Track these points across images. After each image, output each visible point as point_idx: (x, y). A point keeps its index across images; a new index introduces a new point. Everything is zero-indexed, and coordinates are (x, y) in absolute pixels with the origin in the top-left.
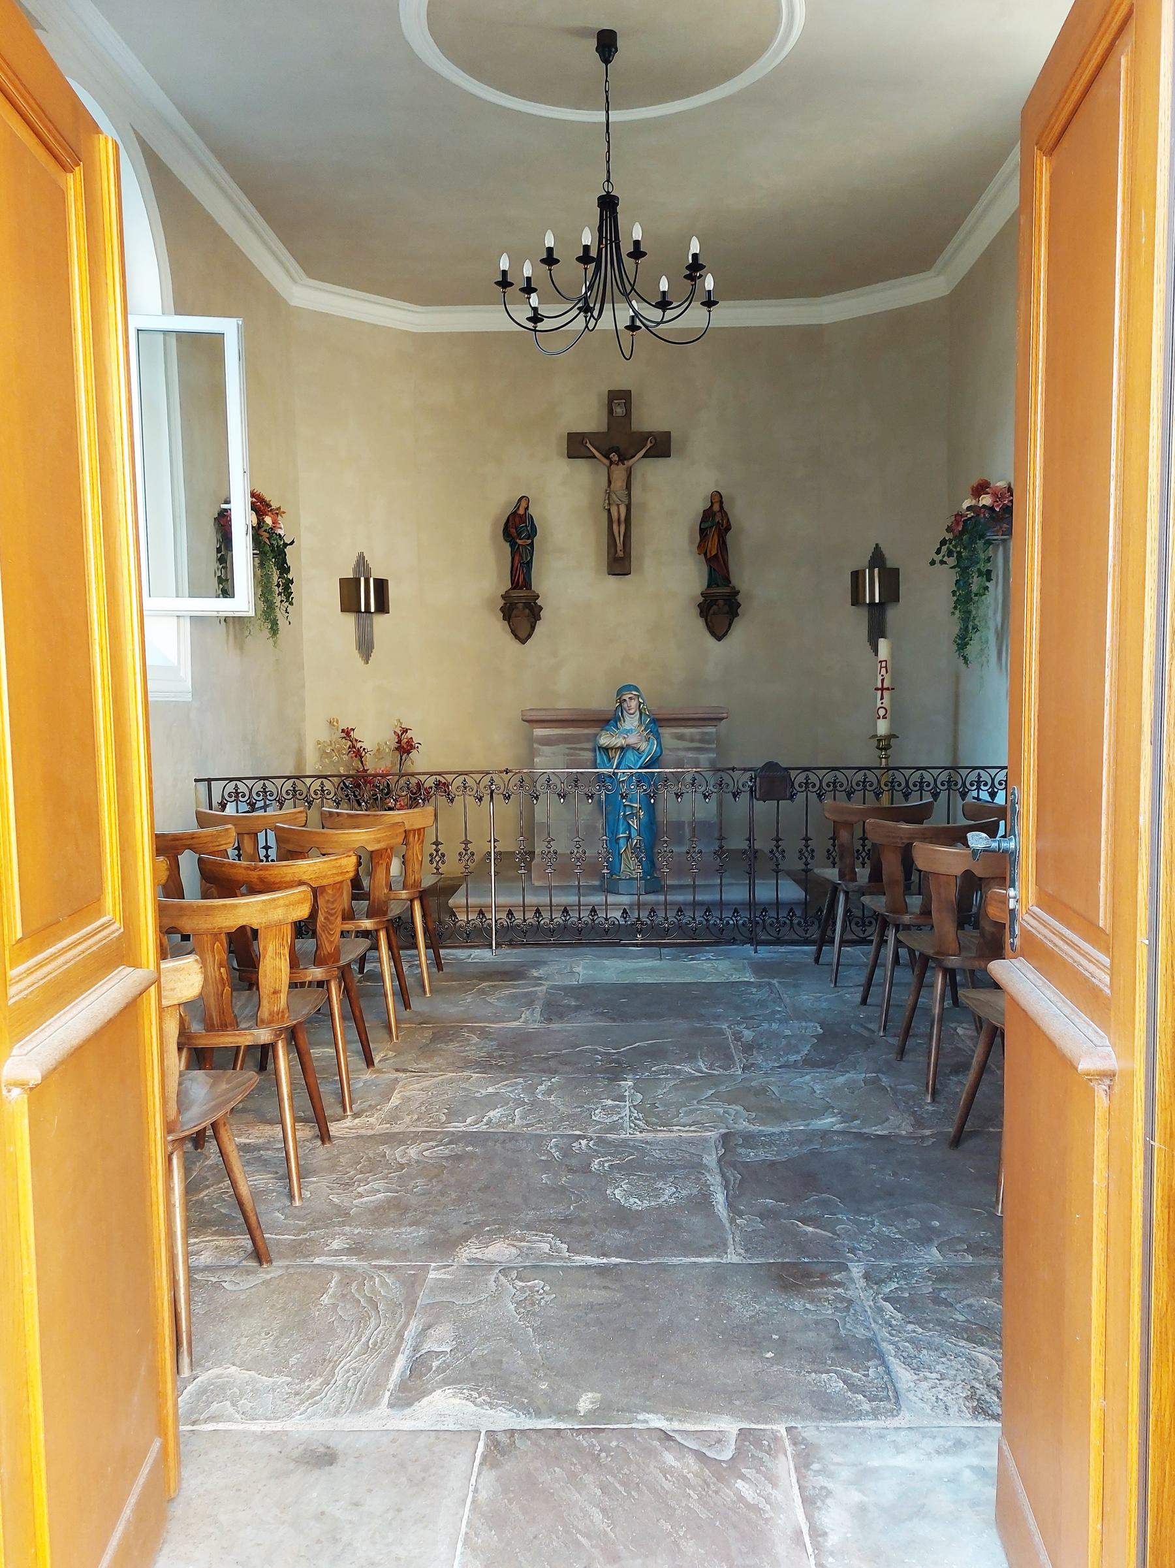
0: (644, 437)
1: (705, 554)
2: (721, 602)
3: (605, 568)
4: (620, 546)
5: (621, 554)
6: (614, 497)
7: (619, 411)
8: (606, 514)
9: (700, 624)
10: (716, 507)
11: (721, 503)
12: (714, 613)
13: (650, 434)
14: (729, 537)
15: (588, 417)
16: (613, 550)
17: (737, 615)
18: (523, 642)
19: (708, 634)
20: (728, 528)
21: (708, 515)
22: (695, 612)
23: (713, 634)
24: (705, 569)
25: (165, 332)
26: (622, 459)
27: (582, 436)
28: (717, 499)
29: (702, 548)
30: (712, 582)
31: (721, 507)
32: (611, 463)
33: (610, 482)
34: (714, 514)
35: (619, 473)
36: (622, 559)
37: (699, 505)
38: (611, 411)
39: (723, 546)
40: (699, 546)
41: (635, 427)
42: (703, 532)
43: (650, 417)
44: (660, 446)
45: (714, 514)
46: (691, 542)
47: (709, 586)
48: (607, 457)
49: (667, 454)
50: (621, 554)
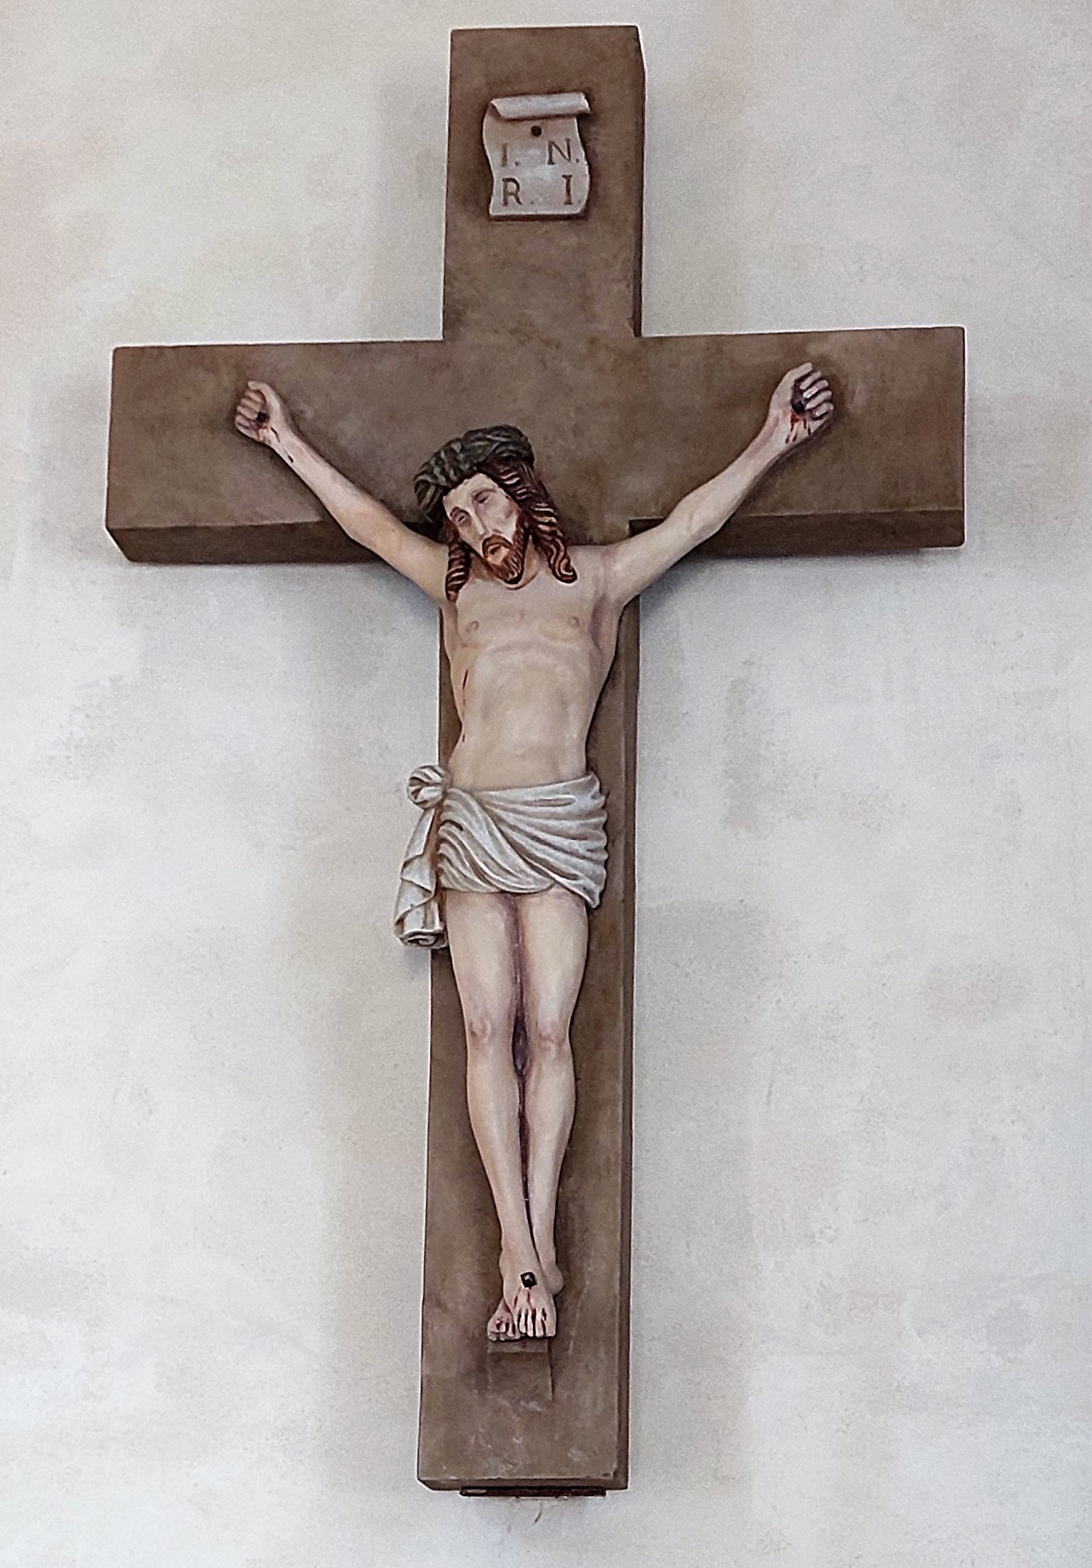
0: (739, 378)
3: (402, 1436)
4: (525, 1245)
5: (530, 1311)
6: (482, 833)
7: (540, 176)
8: (419, 991)
13: (793, 346)
15: (310, 236)
16: (464, 1285)
26: (551, 534)
27: (237, 366)
32: (465, 562)
33: (451, 730)
35: (529, 642)
36: (549, 1352)
38: (471, 181)
41: (675, 308)
43: (782, 230)
44: (867, 466)
48: (432, 524)
49: (918, 522)
50: (530, 1311)
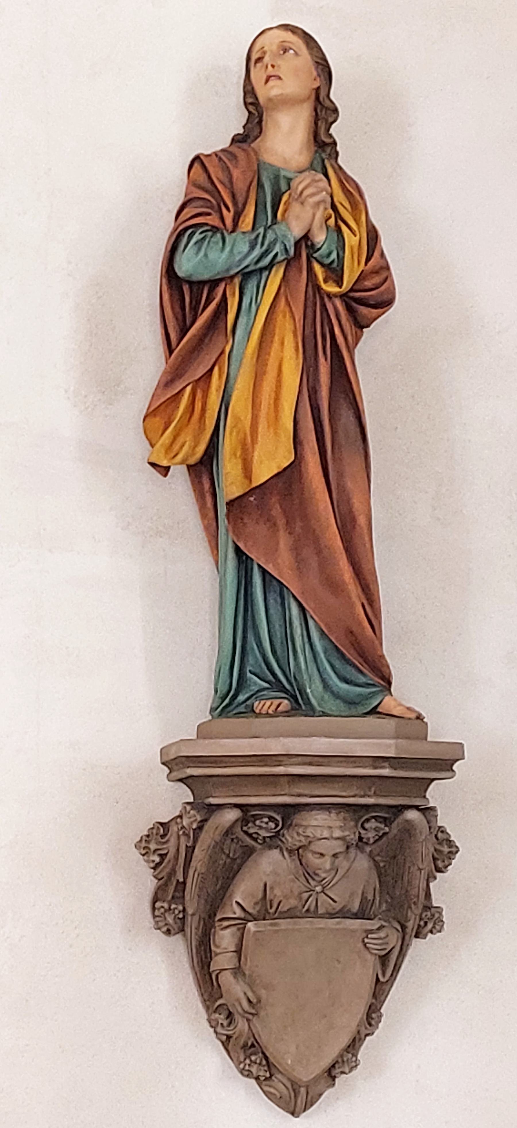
1: (204, 469)
2: (324, 830)
9: (157, 974)
10: (286, 142)
11: (323, 111)
12: (266, 910)
14: (375, 356)
17: (429, 920)
18: (297, 1099)
19: (209, 1060)
20: (370, 299)
21: (221, 191)
22: (129, 886)
23: (252, 1056)
24: (194, 580)
25: (324, 714)
28: (293, 79)
29: (184, 423)
30: (251, 678)
31: (323, 146)
34: (274, 194)
37: (167, 124)
38: (311, 241)
39: (334, 409)
40: (159, 413)
42: (192, 308)
45: (274, 194)
46: (101, 382)
47: (231, 702)
